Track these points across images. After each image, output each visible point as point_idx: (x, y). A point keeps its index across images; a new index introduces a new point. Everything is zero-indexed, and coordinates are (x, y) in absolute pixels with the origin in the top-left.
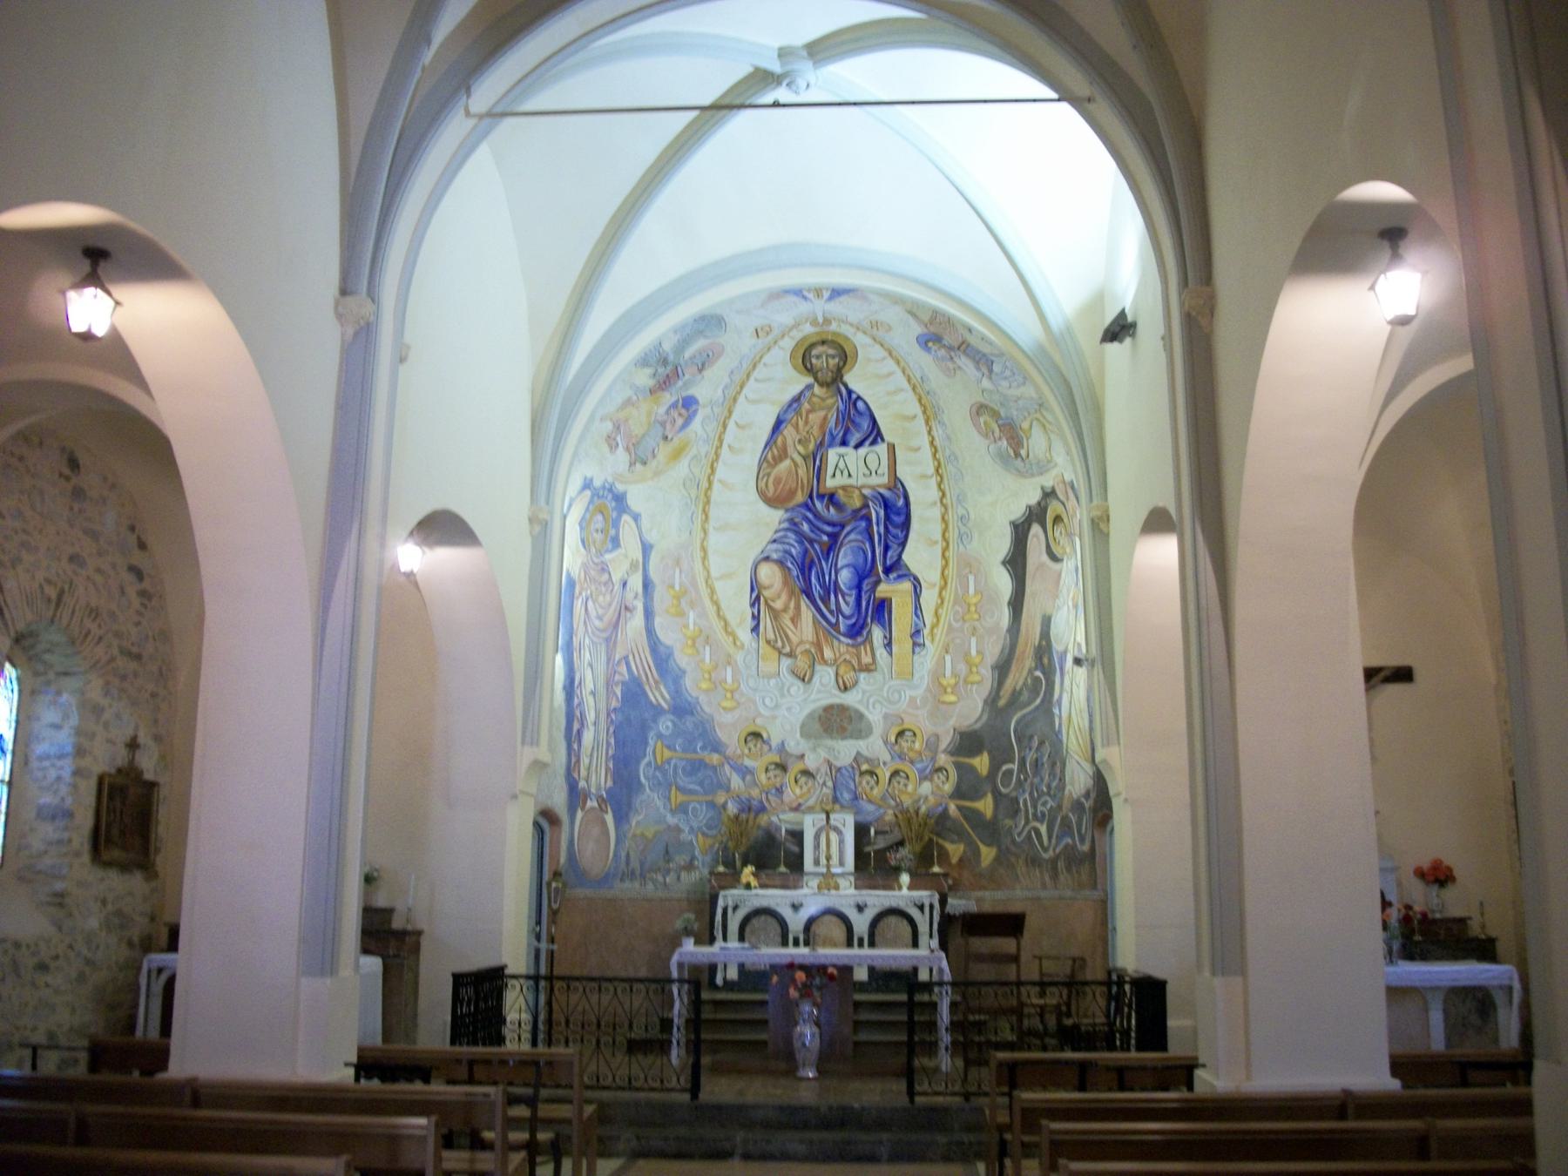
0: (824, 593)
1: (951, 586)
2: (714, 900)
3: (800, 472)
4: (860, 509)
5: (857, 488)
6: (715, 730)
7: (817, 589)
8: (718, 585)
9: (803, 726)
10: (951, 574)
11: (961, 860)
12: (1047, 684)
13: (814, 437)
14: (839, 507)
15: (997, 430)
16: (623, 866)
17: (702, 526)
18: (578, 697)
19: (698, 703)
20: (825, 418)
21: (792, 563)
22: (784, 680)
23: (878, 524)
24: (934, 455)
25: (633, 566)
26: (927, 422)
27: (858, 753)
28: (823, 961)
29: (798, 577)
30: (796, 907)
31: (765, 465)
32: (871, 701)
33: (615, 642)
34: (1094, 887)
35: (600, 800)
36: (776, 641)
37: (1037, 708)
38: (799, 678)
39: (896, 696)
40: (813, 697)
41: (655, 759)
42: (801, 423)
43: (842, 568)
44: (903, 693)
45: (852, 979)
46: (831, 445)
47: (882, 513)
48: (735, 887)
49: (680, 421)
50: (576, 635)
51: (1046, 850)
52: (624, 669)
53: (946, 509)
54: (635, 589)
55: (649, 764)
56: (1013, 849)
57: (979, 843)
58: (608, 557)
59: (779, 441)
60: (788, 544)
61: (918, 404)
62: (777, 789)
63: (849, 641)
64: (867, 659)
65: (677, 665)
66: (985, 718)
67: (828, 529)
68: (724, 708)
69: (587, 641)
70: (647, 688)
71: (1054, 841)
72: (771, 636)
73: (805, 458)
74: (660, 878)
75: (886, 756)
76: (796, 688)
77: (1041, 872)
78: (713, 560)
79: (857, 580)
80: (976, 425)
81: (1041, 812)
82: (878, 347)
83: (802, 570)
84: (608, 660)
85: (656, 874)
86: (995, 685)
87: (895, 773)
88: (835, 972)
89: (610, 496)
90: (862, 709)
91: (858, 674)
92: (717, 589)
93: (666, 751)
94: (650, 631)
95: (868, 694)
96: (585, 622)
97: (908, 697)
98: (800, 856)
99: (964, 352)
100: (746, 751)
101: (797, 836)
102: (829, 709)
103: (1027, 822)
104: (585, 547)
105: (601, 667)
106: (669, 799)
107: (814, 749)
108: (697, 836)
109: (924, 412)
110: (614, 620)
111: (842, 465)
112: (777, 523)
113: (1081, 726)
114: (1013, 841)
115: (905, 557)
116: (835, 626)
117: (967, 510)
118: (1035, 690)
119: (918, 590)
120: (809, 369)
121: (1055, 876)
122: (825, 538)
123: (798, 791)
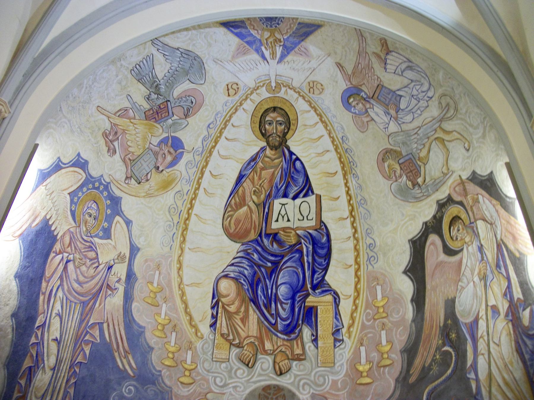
0: (267, 301)
1: (363, 297)
3: (254, 216)
4: (295, 245)
5: (293, 229)
8: (188, 290)
12: (457, 355)
13: (264, 189)
14: (280, 243)
15: (397, 167)
17: (180, 245)
18: (37, 337)
19: (160, 375)
20: (273, 173)
21: (244, 281)
22: (232, 364)
23: (307, 256)
24: (349, 201)
25: (120, 257)
29: (248, 290)
31: (229, 209)
32: (302, 383)
36: (229, 335)
37: (449, 378)
38: (245, 363)
39: (321, 379)
40: (254, 379)
42: (256, 178)
44: (326, 377)
46: (276, 197)
49: (169, 158)
50: (48, 282)
53: (358, 241)
54: (119, 275)
58: (96, 240)
60: (242, 267)
63: (286, 337)
64: (298, 351)
65: (148, 344)
66: (398, 393)
67: (272, 258)
68: (182, 383)
69: (60, 294)
70: (116, 354)
72: (225, 331)
73: (257, 205)
76: (242, 371)
78: (186, 270)
79: (292, 293)
80: (381, 171)
82: (312, 112)
83: (251, 285)
84: (81, 321)
86: (405, 366)
89: (105, 194)
90: (294, 390)
91: (291, 361)
92: (186, 292)
96: (61, 278)
99: (378, 101)
102: (267, 388)
104: (74, 219)
105: (72, 323)
109: (343, 168)
110: (94, 291)
111: (283, 212)
112: (236, 253)
115: (326, 278)
116: (274, 325)
117: (373, 239)
119: (337, 301)
120: (264, 135)
122: (269, 264)
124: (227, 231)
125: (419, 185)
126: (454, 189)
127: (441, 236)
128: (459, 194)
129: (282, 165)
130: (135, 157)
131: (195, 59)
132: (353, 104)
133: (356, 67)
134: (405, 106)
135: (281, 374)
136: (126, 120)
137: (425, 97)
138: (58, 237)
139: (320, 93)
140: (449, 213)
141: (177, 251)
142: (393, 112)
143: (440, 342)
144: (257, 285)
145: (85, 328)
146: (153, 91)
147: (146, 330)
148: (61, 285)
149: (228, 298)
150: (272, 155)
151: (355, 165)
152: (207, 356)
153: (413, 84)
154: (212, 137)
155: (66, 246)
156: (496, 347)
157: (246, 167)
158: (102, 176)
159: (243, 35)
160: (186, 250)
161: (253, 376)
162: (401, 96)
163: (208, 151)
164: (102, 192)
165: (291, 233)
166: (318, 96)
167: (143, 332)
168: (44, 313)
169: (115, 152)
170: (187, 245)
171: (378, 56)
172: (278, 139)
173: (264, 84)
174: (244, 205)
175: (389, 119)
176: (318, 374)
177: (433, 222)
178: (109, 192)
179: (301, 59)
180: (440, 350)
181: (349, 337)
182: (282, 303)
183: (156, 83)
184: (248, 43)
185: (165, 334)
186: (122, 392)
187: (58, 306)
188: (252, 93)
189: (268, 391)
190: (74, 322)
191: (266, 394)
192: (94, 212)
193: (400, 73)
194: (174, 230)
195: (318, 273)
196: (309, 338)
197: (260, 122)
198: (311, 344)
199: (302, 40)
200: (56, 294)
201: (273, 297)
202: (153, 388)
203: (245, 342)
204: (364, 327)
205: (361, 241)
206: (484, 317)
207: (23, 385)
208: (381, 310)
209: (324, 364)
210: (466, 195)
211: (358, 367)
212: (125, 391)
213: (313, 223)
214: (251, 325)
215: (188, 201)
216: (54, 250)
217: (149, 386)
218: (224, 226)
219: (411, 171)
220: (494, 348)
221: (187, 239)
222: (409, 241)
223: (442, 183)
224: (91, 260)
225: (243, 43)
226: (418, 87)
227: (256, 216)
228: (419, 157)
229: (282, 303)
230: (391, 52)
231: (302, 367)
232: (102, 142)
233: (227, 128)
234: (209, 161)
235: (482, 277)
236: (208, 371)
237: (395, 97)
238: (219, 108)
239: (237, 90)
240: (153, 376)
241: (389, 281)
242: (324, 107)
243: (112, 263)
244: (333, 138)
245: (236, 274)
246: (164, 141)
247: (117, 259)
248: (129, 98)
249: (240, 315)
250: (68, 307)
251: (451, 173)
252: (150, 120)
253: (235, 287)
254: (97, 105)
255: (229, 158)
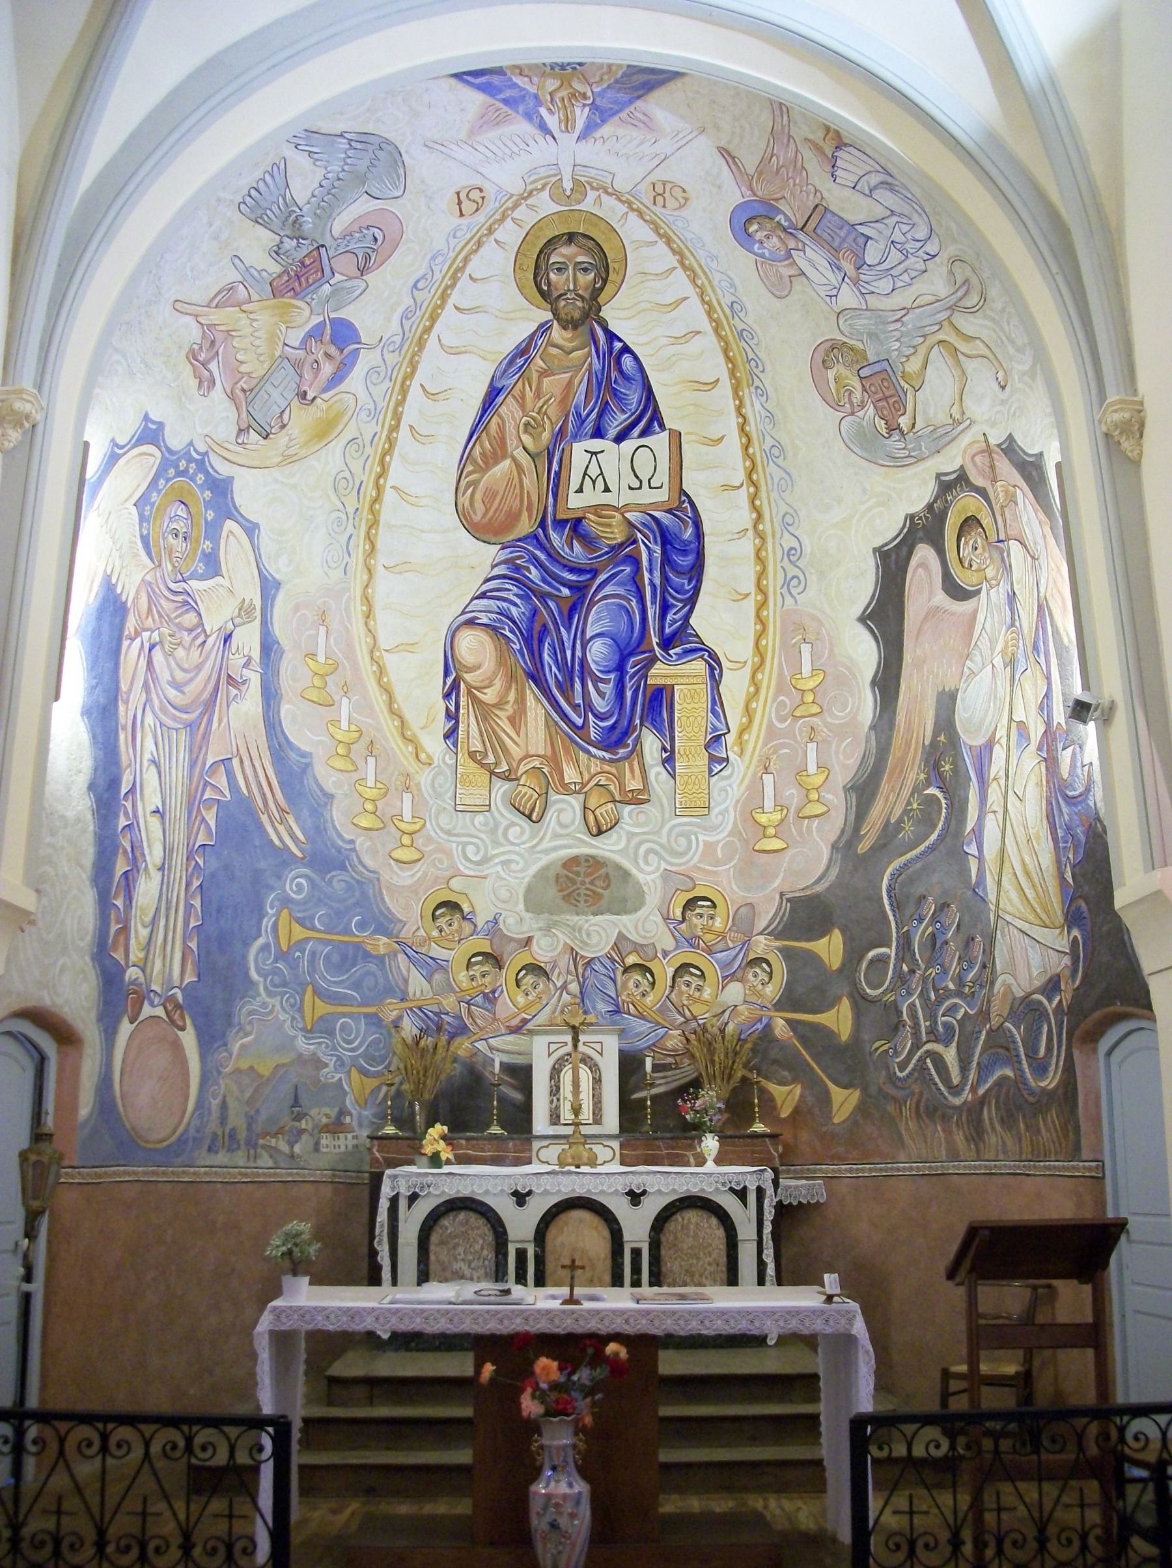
0: (564, 677)
2: (376, 1181)
3: (526, 481)
4: (621, 545)
5: (617, 509)
6: (383, 899)
7: (552, 672)
8: (390, 661)
9: (529, 891)
10: (770, 644)
11: (796, 1111)
12: (950, 806)
13: (549, 418)
14: (589, 541)
15: (856, 383)
16: (213, 1125)
17: (365, 561)
18: (126, 814)
19: (354, 850)
20: (570, 383)
21: (512, 631)
23: (651, 571)
25: (245, 610)
26: (736, 390)
27: (621, 936)
28: (593, 1326)
30: (521, 1198)
31: (469, 468)
33: (206, 735)
34: (1075, 1152)
35: (171, 1004)
37: (932, 848)
38: (523, 814)
39: (683, 841)
40: (545, 845)
41: (277, 937)
42: (529, 394)
43: (592, 638)
44: (693, 837)
45: (656, 1371)
46: (576, 437)
47: (658, 549)
48: (410, 1163)
49: (327, 369)
50: (127, 702)
51: (956, 1090)
52: (222, 781)
53: (763, 539)
55: (265, 948)
56: (891, 1090)
57: (831, 1085)
58: (195, 584)
59: (493, 426)
61: (721, 358)
62: (485, 995)
63: (607, 755)
64: (634, 784)
65: (322, 790)
69: (149, 719)
70: (264, 818)
71: (972, 1075)
72: (477, 745)
74: (284, 1147)
75: (667, 942)
77: (948, 1132)
78: (382, 618)
79: (617, 657)
81: (945, 1024)
82: (661, 246)
83: (528, 641)
84: (193, 764)
85: (278, 1139)
86: (852, 818)
87: (683, 968)
88: (623, 1353)
89: (200, 478)
90: (627, 864)
92: (388, 665)
93: (296, 927)
94: (272, 724)
95: (636, 840)
96: (146, 686)
97: (701, 844)
98: (526, 1109)
99: (815, 235)
100: (435, 933)
101: (521, 1075)
102: (572, 863)
103: (916, 1046)
104: (149, 554)
105: (178, 774)
106: (301, 1009)
107: (547, 929)
108: (349, 1073)
109: (732, 373)
110: (206, 695)
111: (594, 471)
113: (1030, 867)
114: (892, 1079)
115: (692, 621)
118: (927, 820)
119: (716, 673)
121: (977, 1133)
122: (566, 592)
123: (521, 1000)
124: (466, 519)
125: (902, 432)
126: (973, 457)
127: (941, 552)
128: (982, 473)
129: (591, 364)
130: (255, 382)
131: (381, 149)
132: (759, 236)
133: (765, 161)
134: (877, 261)
135: (600, 832)
136: (232, 309)
137: (921, 252)
138: (129, 604)
139: (681, 207)
140: (959, 506)
141: (358, 575)
142: (849, 267)
143: (922, 776)
144: (541, 641)
145: (201, 776)
146: (288, 233)
147: (315, 760)
148: (148, 700)
149: (479, 672)
150: (565, 339)
151: (761, 368)
152: (444, 801)
153: (895, 219)
154: (423, 308)
155: (144, 617)
156: (1018, 803)
157: (505, 371)
158: (191, 444)
159: (495, 87)
160: (380, 571)
161: (542, 839)
162: (868, 238)
163: (415, 340)
164: (193, 479)
165: (613, 517)
166: (676, 213)
167: (308, 765)
168: (130, 765)
169: (213, 382)
170: (381, 560)
171: (819, 150)
172: (579, 304)
173: (544, 186)
174: (504, 457)
175: (840, 279)
176: (677, 830)
177: (927, 518)
178: (207, 473)
179: (635, 134)
180: (920, 794)
181: (741, 754)
182: (596, 680)
183: (293, 216)
184: (506, 102)
185: (353, 763)
186: (285, 891)
187: (150, 745)
188: (516, 206)
189: (575, 869)
190: (180, 769)
191: (571, 875)
192: (182, 524)
193: (867, 192)
194: (350, 529)
195: (675, 610)
196: (657, 755)
197: (537, 267)
198: (661, 769)
199: (639, 97)
200: (142, 722)
201: (577, 667)
202: (343, 876)
203: (522, 769)
204: (772, 733)
205: (769, 540)
206: (1004, 741)
207: (121, 907)
208: (809, 698)
209: (688, 810)
210: (994, 480)
211: (757, 816)
212: (291, 889)
213: (662, 496)
214: (531, 730)
215: (374, 459)
216: (126, 633)
217: (334, 873)
218: (460, 507)
219: (886, 398)
220: (1013, 804)
221: (379, 545)
222: (875, 550)
223: (947, 439)
224: (190, 631)
225: (494, 102)
226: (905, 228)
227: (531, 482)
228: (903, 372)
229: (596, 680)
230: (846, 145)
231: (642, 817)
232: (187, 371)
233: (459, 285)
234: (418, 362)
235: (1008, 660)
236: (448, 833)
237: (852, 236)
238: (440, 243)
239: (480, 201)
240: (340, 852)
241: (829, 635)
242: (689, 236)
243: (230, 626)
244: (709, 304)
245: (494, 616)
246: (315, 334)
247: (239, 615)
248: (237, 261)
249: (506, 710)
250: (166, 742)
251: (968, 422)
252: (283, 296)
253: (492, 648)
254: (172, 299)
255: (465, 352)
